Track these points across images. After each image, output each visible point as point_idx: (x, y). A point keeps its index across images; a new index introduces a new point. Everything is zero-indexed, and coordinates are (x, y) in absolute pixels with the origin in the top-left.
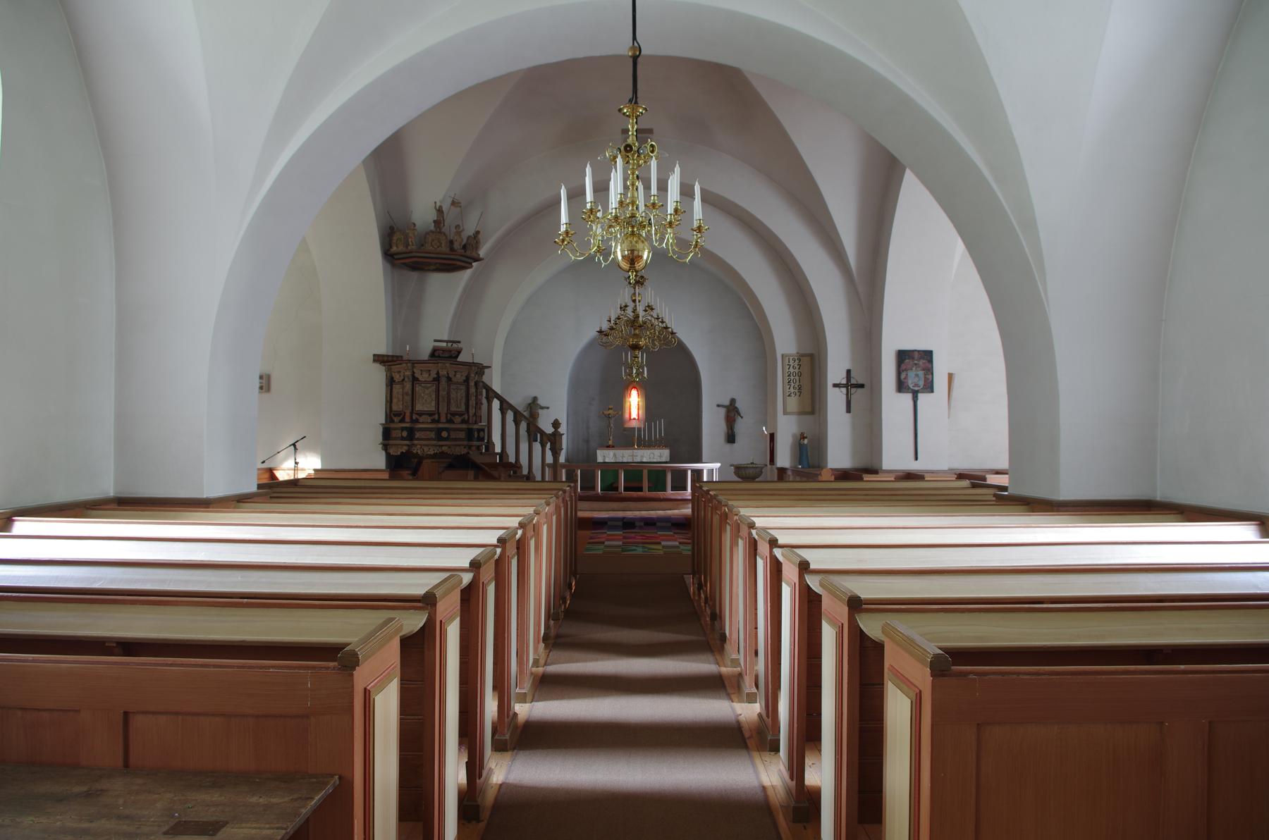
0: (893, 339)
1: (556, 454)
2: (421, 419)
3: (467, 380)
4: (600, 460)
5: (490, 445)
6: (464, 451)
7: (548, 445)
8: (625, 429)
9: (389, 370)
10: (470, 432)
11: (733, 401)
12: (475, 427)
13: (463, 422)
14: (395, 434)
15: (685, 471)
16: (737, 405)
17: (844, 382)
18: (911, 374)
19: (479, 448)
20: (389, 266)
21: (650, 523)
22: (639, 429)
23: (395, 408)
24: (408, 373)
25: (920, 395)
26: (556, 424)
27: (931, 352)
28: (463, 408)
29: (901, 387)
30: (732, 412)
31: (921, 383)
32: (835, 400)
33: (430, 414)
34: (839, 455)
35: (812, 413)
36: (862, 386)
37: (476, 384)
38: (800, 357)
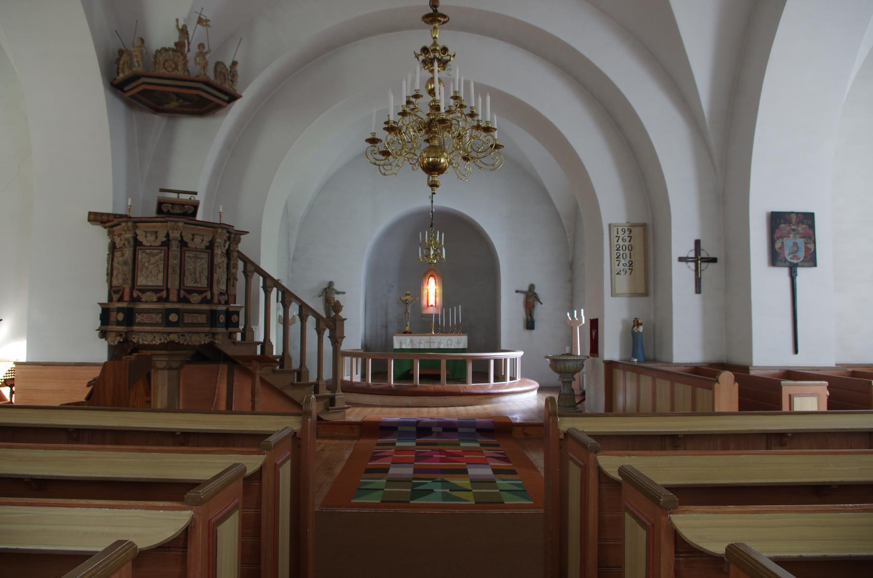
0: (767, 195)
1: (336, 340)
2: (144, 297)
3: (211, 247)
4: (396, 346)
6: (205, 340)
7: (327, 332)
8: (423, 316)
9: (111, 234)
10: (213, 317)
11: (532, 287)
13: (204, 301)
14: (113, 317)
15: (487, 362)
16: (536, 291)
17: (692, 255)
18: (788, 243)
19: (231, 336)
20: (120, 106)
21: (449, 428)
22: (437, 316)
23: (115, 283)
24: (129, 235)
25: (800, 270)
28: (204, 283)
29: (775, 259)
30: (531, 298)
31: (801, 255)
32: (682, 277)
33: (156, 290)
35: (646, 294)
36: (714, 260)
37: (228, 254)
38: (631, 228)
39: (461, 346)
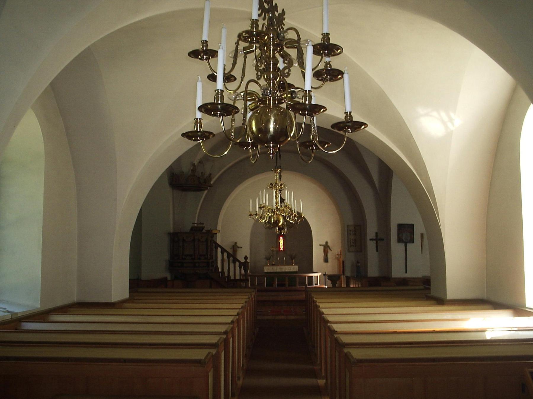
0: (397, 218)
4: (266, 271)
5: (217, 268)
11: (327, 243)
12: (211, 261)
16: (329, 244)
17: (375, 238)
25: (408, 244)
26: (246, 258)
27: (413, 225)
29: (400, 240)
31: (409, 239)
32: (371, 246)
34: (373, 271)
36: (383, 240)
39: (295, 270)
